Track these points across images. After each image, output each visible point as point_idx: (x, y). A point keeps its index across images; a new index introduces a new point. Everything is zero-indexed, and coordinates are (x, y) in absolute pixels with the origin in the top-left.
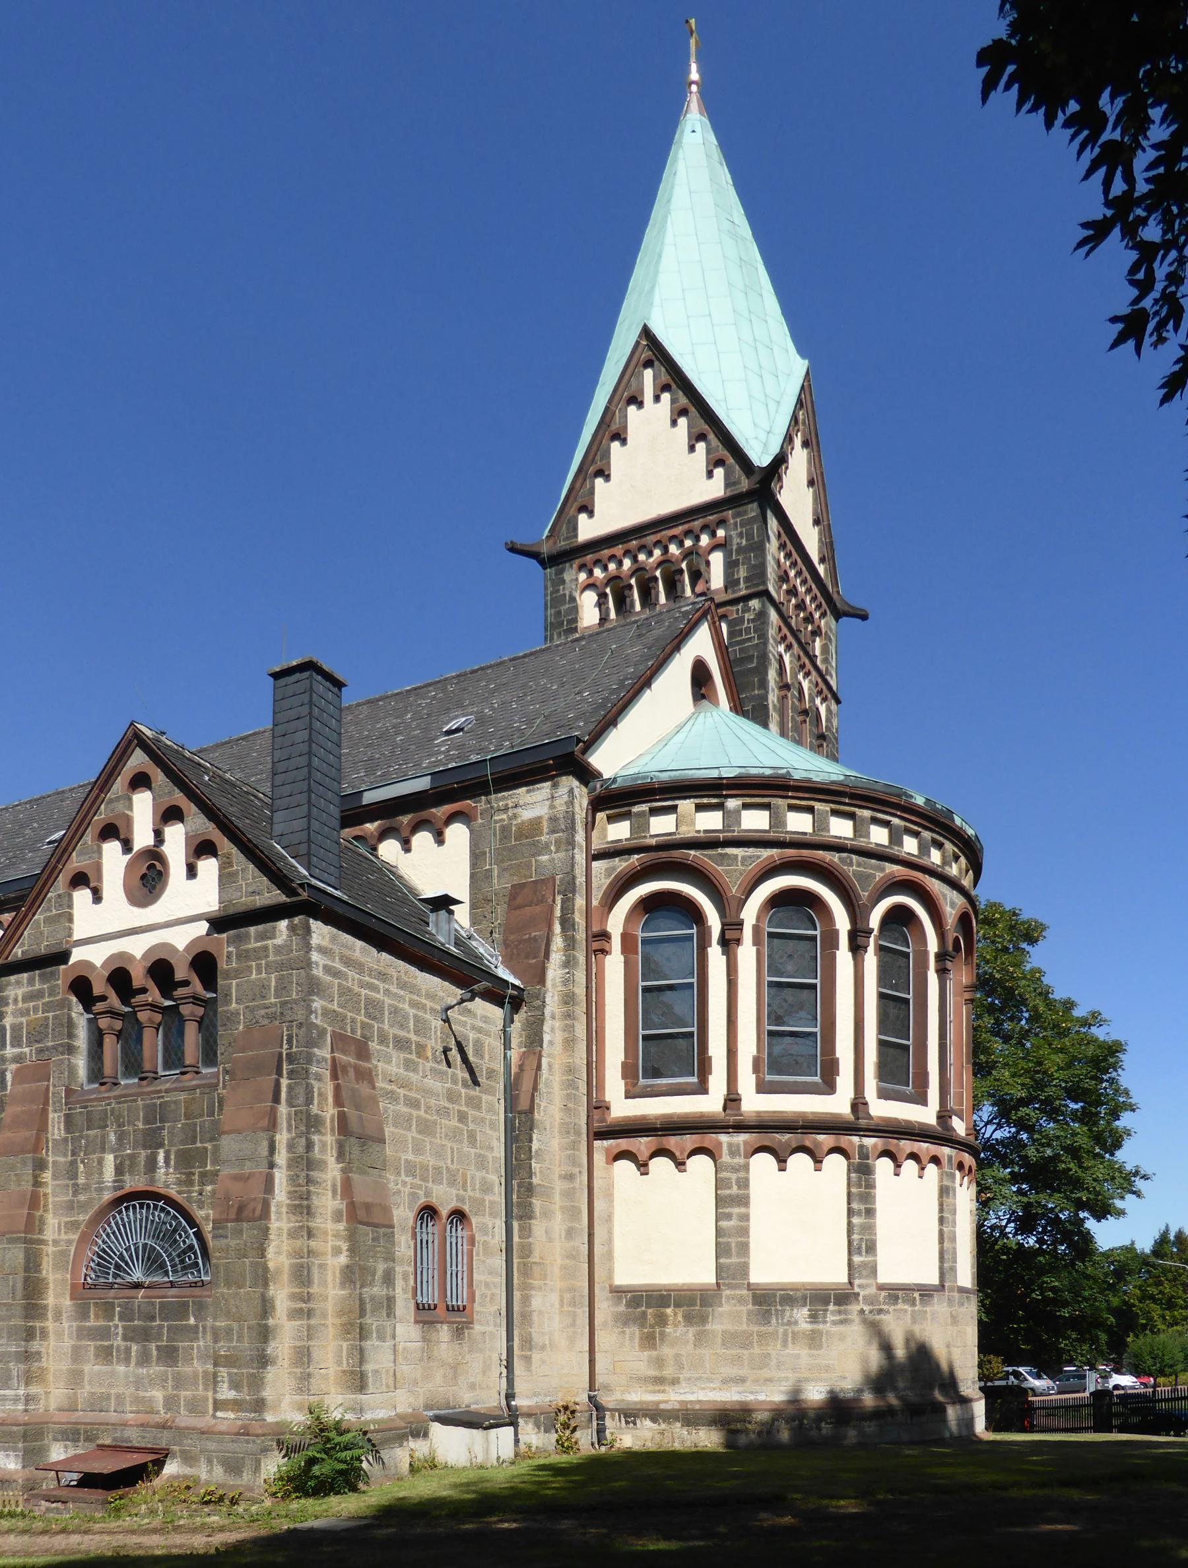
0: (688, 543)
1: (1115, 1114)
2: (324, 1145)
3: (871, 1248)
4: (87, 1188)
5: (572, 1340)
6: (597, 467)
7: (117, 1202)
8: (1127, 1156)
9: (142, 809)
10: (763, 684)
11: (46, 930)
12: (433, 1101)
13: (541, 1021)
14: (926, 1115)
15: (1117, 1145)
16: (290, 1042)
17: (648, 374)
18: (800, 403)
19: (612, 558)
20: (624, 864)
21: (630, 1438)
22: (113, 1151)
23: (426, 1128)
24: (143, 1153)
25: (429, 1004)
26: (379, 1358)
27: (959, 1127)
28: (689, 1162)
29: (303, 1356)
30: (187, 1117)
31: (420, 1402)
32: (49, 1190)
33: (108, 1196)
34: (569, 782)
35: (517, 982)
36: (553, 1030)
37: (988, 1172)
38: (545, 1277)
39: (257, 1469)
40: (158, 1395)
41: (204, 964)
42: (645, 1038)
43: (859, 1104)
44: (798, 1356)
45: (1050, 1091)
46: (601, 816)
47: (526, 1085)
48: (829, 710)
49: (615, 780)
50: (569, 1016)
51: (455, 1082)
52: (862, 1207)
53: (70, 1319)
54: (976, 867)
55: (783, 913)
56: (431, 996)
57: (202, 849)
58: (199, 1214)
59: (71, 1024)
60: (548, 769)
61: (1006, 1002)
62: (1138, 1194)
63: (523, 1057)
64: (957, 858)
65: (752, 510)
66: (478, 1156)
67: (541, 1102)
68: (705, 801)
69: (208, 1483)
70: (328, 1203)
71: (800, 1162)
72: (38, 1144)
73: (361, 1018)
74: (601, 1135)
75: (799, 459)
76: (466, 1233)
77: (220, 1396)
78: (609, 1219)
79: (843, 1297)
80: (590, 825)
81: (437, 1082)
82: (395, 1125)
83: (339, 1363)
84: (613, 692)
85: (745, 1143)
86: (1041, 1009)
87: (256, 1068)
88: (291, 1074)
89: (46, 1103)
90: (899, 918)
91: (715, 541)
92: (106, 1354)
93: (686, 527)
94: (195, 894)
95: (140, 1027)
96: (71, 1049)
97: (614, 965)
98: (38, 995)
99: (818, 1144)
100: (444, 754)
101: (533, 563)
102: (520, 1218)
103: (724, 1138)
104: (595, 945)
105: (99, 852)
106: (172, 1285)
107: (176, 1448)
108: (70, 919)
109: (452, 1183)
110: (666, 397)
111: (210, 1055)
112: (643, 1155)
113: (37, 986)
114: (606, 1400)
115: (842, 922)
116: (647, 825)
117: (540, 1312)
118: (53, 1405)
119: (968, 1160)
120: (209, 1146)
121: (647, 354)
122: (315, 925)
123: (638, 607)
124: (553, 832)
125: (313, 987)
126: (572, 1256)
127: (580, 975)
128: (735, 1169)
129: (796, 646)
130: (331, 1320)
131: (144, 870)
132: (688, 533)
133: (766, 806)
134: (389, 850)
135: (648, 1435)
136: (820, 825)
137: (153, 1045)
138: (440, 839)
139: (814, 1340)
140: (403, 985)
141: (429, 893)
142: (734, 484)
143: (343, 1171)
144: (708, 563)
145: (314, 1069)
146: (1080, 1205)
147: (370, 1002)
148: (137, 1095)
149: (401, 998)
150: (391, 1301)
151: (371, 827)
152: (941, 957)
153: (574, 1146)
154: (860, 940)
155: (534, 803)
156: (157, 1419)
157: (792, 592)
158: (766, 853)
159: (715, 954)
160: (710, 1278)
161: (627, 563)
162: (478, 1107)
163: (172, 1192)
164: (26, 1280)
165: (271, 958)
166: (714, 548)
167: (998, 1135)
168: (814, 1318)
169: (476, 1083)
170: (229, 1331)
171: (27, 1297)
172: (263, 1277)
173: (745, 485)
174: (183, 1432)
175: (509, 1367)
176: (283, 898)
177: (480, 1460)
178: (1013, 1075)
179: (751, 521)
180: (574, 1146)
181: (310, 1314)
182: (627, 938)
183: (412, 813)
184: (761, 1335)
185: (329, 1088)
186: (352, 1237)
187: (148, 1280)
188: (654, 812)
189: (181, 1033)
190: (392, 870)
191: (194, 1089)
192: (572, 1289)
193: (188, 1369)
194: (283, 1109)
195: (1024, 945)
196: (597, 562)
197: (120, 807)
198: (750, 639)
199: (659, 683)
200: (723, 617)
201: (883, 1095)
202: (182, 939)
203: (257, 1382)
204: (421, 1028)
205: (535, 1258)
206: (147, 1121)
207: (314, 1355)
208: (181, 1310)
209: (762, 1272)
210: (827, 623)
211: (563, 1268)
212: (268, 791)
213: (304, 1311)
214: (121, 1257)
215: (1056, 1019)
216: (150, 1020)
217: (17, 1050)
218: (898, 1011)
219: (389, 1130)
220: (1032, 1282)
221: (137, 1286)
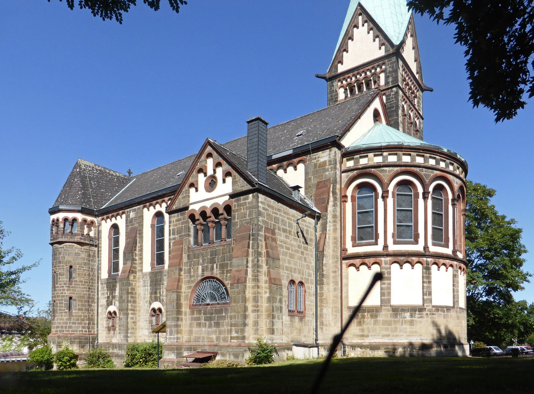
0: (373, 71)
1: (519, 254)
2: (262, 260)
3: (430, 294)
4: (194, 276)
5: (335, 323)
6: (344, 48)
7: (203, 280)
8: (524, 269)
10: (397, 115)
11: (182, 200)
12: (294, 248)
13: (326, 223)
14: (448, 251)
15: (521, 265)
18: (410, 23)
19: (349, 77)
20: (352, 174)
22: (201, 265)
23: (292, 256)
24: (210, 265)
25: (292, 218)
26: (278, 325)
27: (460, 255)
29: (256, 323)
30: (223, 254)
31: (290, 340)
32: (183, 277)
33: (200, 278)
34: (335, 149)
35: (319, 212)
36: (330, 226)
37: (475, 274)
38: (327, 303)
39: (243, 356)
40: (214, 337)
41: (228, 208)
42: (359, 228)
43: (426, 248)
44: (406, 328)
45: (496, 246)
46: (345, 159)
47: (322, 243)
48: (420, 122)
49: (349, 148)
50: (335, 221)
51: (300, 242)
52: (427, 281)
53: (189, 315)
54: (465, 171)
55: (400, 188)
56: (293, 216)
57: (227, 174)
58: (226, 282)
59: (189, 228)
60: (328, 145)
61: (480, 216)
62: (528, 281)
63: (321, 235)
64: (458, 168)
65: (394, 59)
66: (307, 265)
68: (377, 153)
69: (229, 361)
70: (263, 278)
71: (407, 266)
72: (180, 264)
73: (273, 223)
75: (410, 41)
76: (303, 289)
77: (232, 336)
78: (347, 285)
79: (421, 309)
80: (341, 162)
81: (295, 242)
82: (283, 255)
83: (266, 326)
84: (348, 121)
85: (390, 260)
86: (493, 219)
87: (243, 238)
89: (182, 251)
90: (439, 188)
91: (382, 70)
92: (199, 325)
93: (372, 66)
94: (225, 188)
95: (209, 228)
96: (189, 235)
97: (349, 206)
99: (412, 260)
100: (297, 143)
102: (320, 284)
103: (383, 259)
104: (343, 200)
105: (197, 177)
106: (218, 304)
107: (219, 352)
108: (189, 197)
109: (299, 273)
110: (366, 24)
111: (229, 236)
115: (420, 190)
117: (326, 314)
118: (184, 341)
119: (463, 266)
120: (229, 262)
121: (360, 11)
122: (260, 195)
123: (357, 92)
124: (330, 165)
125: (259, 214)
126: (336, 297)
127: (338, 209)
128: (386, 269)
129: (408, 102)
130: (264, 313)
131: (210, 181)
132: (373, 68)
133: (396, 154)
134: (280, 173)
135: (359, 353)
136: (413, 159)
137: (213, 233)
138: (295, 169)
139: (412, 323)
140: (285, 213)
141: (292, 185)
142: (388, 51)
143: (268, 268)
144: (379, 77)
145: (259, 238)
146: (508, 285)
147: (275, 218)
148: (208, 248)
149: (284, 217)
150: (281, 307)
151: (275, 166)
152: (453, 200)
153: (336, 262)
154: (426, 195)
155: (324, 156)
156: (214, 343)
157: (407, 84)
158: (396, 169)
159: (380, 201)
161: (354, 79)
162: (307, 250)
163: (218, 276)
164: (177, 303)
165: (247, 206)
166: (381, 72)
167: (479, 262)
168: (411, 316)
169: (307, 243)
170: (235, 316)
171: (177, 308)
172: (245, 300)
173: (391, 51)
174: (221, 347)
175: (316, 331)
176: (251, 188)
177: (307, 357)
178: (484, 241)
179: (393, 63)
180: (336, 262)
181: (258, 311)
182: (353, 198)
183: (286, 161)
184: (394, 321)
185: (264, 243)
186: (270, 288)
187: (211, 303)
188: (361, 157)
189: (221, 229)
190: (281, 179)
191: (224, 245)
192: (335, 307)
194: (251, 250)
195: (488, 197)
196: (344, 79)
197: (203, 163)
198: (393, 101)
199: (362, 118)
200: (384, 94)
201: (434, 245)
202: (221, 201)
203: (243, 331)
204: (290, 226)
205: (324, 297)
206: (211, 256)
207: (259, 323)
208: (221, 311)
209: (396, 301)
210: (419, 93)
211: (333, 300)
212: (246, 157)
213: (256, 310)
214: (203, 296)
215: (499, 222)
216: (212, 226)
217: (174, 236)
218: (439, 218)
219: (281, 257)
220: (490, 311)
221: (208, 305)
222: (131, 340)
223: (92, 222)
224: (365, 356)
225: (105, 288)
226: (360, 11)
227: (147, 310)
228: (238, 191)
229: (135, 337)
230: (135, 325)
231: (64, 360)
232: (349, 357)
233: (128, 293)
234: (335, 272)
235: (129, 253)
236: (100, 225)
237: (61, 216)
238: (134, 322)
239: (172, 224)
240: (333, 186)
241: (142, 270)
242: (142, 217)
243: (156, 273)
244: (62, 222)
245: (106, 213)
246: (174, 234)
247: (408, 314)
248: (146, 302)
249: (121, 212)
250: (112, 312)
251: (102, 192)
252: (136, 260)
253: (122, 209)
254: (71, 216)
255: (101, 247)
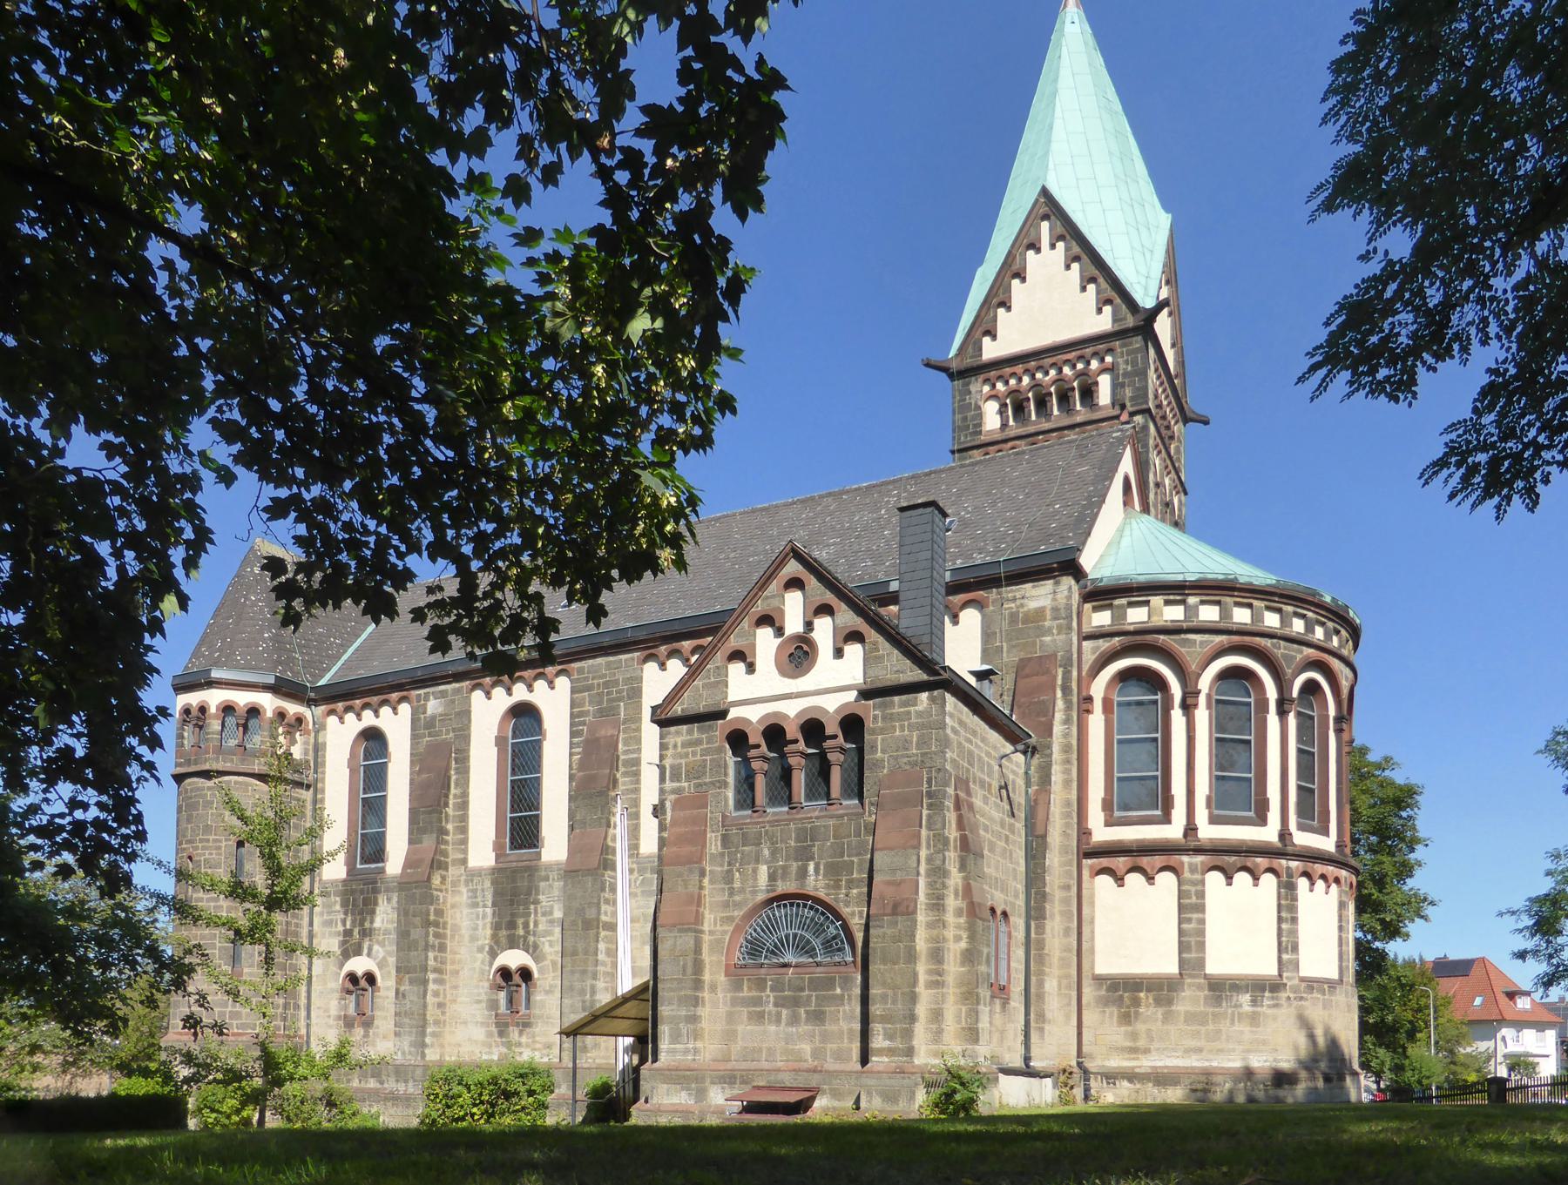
0: (1080, 366)
3: (1295, 948)
4: (742, 890)
5: (1068, 1017)
6: (999, 298)
7: (770, 901)
8: (1417, 883)
9: (793, 609)
16: (929, 782)
17: (1045, 225)
19: (1013, 374)
21: (1111, 1097)
22: (766, 863)
28: (1158, 877)
29: (937, 1015)
33: (761, 897)
34: (1068, 581)
40: (806, 1048)
41: (852, 725)
42: (1120, 779)
46: (1088, 606)
58: (845, 911)
60: (1053, 570)
62: (1425, 918)
65: (1137, 342)
67: (1050, 829)
70: (952, 903)
71: (1242, 878)
74: (1088, 855)
78: (1092, 921)
79: (1275, 986)
83: (959, 1022)
88: (930, 807)
90: (1311, 688)
92: (759, 1017)
97: (1096, 722)
98: (698, 742)
99: (1257, 865)
101: (944, 375)
102: (1037, 919)
103: (1185, 859)
106: (818, 964)
112: (1121, 871)
113: (696, 735)
114: (1089, 1065)
115: (1272, 693)
116: (1125, 617)
118: (708, 1057)
120: (855, 859)
121: (1044, 210)
122: (948, 696)
123: (1033, 417)
124: (1056, 619)
128: (1194, 883)
132: (1080, 358)
133: (1218, 603)
135: (1125, 1093)
136: (1257, 618)
139: (1254, 1019)
143: (966, 879)
144: (1096, 383)
153: (1069, 863)
154: (1286, 707)
155: (1039, 596)
156: (805, 1065)
158: (1218, 639)
159: (1177, 716)
160: (1172, 968)
161: (1026, 380)
163: (821, 894)
165: (913, 720)
168: (1254, 1002)
172: (912, 957)
173: (1130, 321)
176: (925, 677)
179: (1136, 351)
182: (1107, 704)
184: (1214, 1015)
186: (971, 930)
188: (1131, 604)
191: (842, 816)
193: (834, 1028)
196: (1000, 378)
201: (1301, 828)
202: (832, 705)
203: (908, 1034)
206: (798, 840)
208: (829, 983)
210: (1178, 428)
219: (986, 852)
222: (432, 1055)
223: (300, 720)
224: (1142, 1101)
225: (338, 907)
226: (1044, 210)
227: (482, 972)
228: (889, 683)
229: (442, 1046)
230: (443, 1013)
231: (225, 1109)
232: (311, 1124)
233: (427, 924)
234: (1067, 888)
235: (430, 813)
236: (320, 727)
237: (214, 698)
238: (440, 1005)
239: (670, 752)
240: (1064, 674)
241: (464, 861)
242: (466, 714)
243: (515, 871)
244: (216, 716)
245: (343, 695)
246: (676, 776)
247: (1245, 999)
248: (480, 950)
249: (395, 696)
250: (360, 973)
251: (320, 634)
252: (447, 833)
253: (399, 687)
254: (242, 698)
255: (323, 791)
